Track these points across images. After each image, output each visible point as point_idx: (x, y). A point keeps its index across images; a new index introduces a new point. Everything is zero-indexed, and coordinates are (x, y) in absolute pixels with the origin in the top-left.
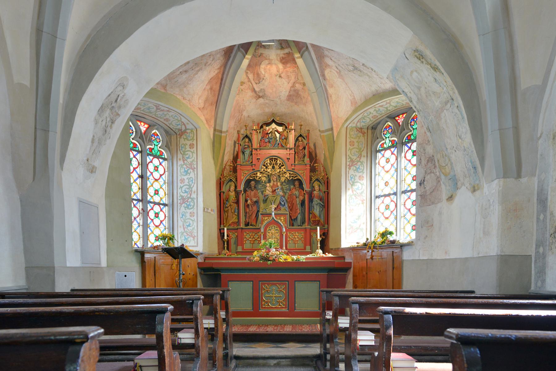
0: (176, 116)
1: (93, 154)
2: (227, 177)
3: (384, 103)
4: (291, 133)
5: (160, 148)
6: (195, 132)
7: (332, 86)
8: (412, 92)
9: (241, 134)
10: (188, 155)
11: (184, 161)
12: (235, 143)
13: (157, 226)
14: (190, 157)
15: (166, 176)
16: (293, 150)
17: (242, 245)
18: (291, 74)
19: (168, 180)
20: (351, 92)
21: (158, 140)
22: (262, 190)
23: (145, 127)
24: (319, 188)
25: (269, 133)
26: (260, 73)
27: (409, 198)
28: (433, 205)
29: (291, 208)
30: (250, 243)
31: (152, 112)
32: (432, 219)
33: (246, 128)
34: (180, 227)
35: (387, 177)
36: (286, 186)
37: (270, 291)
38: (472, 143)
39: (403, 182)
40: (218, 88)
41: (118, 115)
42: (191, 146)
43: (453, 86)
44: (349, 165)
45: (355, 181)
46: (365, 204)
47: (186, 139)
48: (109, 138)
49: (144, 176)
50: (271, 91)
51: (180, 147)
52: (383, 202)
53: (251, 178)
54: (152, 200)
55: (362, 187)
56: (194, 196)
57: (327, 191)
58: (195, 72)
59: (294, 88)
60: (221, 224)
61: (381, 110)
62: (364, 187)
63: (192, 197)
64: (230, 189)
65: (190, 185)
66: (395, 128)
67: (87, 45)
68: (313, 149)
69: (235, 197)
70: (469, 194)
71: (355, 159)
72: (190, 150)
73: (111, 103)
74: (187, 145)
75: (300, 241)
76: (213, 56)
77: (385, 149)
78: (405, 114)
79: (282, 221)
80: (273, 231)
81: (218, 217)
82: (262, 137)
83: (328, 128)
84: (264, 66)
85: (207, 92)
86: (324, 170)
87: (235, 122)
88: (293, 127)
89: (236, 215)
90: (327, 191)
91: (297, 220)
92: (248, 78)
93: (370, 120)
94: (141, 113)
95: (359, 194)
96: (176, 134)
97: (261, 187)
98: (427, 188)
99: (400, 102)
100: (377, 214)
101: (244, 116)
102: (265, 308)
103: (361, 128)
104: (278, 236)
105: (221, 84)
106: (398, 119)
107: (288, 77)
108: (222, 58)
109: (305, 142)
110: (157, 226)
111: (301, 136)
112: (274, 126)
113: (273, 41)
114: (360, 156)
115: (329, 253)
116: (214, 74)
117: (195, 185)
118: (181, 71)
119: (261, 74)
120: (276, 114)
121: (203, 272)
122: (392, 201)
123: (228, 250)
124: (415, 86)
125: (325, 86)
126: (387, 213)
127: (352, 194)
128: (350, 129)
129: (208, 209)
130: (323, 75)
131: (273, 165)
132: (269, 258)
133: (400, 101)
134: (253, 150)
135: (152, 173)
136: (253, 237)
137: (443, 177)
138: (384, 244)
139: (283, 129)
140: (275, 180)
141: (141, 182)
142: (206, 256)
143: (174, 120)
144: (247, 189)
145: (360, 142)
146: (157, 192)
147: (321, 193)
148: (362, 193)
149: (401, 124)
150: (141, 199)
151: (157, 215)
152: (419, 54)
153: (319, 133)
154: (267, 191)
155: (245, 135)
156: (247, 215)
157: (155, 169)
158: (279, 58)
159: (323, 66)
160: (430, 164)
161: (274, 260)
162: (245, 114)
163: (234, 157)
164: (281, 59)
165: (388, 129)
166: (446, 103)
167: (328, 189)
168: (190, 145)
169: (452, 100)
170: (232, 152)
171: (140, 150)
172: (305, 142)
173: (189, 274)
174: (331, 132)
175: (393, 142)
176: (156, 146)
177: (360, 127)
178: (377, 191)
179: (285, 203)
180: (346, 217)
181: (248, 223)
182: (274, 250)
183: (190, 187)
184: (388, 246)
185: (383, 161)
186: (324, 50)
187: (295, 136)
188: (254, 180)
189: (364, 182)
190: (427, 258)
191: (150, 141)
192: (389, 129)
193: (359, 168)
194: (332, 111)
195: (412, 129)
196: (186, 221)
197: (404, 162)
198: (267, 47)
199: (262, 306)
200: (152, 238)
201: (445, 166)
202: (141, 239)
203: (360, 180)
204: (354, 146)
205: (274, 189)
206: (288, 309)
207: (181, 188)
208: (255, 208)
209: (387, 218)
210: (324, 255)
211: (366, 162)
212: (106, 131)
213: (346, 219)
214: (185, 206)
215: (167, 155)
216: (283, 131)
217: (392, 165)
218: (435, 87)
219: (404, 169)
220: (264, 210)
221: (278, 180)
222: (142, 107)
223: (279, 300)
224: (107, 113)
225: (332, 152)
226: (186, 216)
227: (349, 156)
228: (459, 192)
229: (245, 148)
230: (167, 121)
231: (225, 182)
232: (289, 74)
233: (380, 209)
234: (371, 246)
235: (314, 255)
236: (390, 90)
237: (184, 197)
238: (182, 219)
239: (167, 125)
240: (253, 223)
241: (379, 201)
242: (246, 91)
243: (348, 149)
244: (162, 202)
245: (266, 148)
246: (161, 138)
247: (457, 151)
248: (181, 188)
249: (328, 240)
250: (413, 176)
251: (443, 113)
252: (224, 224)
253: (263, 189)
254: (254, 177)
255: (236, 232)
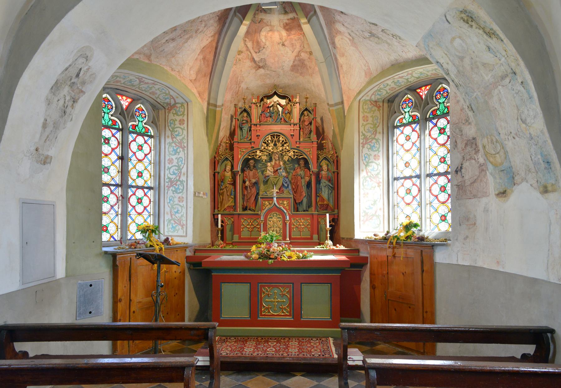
0: (163, 89)
1: (45, 141)
2: (222, 155)
3: (405, 74)
4: (295, 106)
5: (145, 124)
6: (186, 106)
7: (343, 55)
8: (450, 63)
9: (238, 108)
10: (178, 132)
11: (172, 138)
12: (232, 117)
13: (139, 214)
14: (180, 134)
15: (152, 155)
16: (298, 125)
17: (239, 233)
18: (296, 42)
19: (155, 160)
20: (365, 62)
21: (143, 116)
22: (262, 169)
23: (127, 102)
24: (328, 168)
25: (271, 107)
26: (259, 40)
27: (436, 182)
28: (476, 199)
29: (295, 190)
30: (248, 231)
31: (134, 84)
32: (475, 216)
33: (244, 101)
34: (167, 213)
35: (407, 157)
36: (290, 165)
37: (271, 294)
38: (545, 130)
39: (428, 163)
40: (212, 58)
41: (82, 92)
42: (181, 122)
43: (518, 56)
44: (362, 143)
45: (370, 161)
46: (381, 187)
47: (175, 114)
48: (70, 120)
49: (125, 157)
50: (272, 61)
51: (169, 123)
52: (403, 185)
53: (250, 157)
54: (134, 184)
55: (378, 167)
56: (183, 178)
57: (337, 171)
58: (184, 40)
59: (298, 58)
60: (215, 209)
61: (400, 82)
62: (380, 168)
63: (181, 179)
64: (226, 168)
65: (179, 166)
66: (417, 101)
67: (32, 6)
68: (320, 124)
69: (231, 177)
70: (536, 194)
71: (370, 136)
72: (180, 126)
73: (70, 79)
74: (176, 120)
75: (306, 228)
76: (205, 22)
77: (405, 125)
78: (429, 86)
79: (285, 205)
80: (274, 219)
81: (211, 202)
82: (263, 112)
83: (338, 101)
84: (265, 33)
85: (199, 62)
86: (332, 148)
87: (232, 95)
88: (297, 100)
89: (232, 198)
90: (337, 171)
91: (302, 205)
92: (247, 46)
93: (387, 93)
94: (122, 86)
95: (374, 176)
96: (165, 108)
97: (261, 166)
98: (466, 177)
99: (424, 73)
100: (396, 199)
101: (242, 88)
102: (265, 315)
103: (376, 102)
104: (281, 224)
105: (215, 53)
106: (420, 92)
107: (293, 45)
108: (216, 25)
109: (312, 117)
110: (139, 214)
111: (306, 109)
112: (276, 98)
113: (275, 3)
114: (375, 133)
115: (340, 244)
116: (207, 42)
117: (185, 166)
118: (167, 39)
119: (262, 42)
120: (278, 86)
121: (192, 267)
122: (414, 185)
123: (223, 240)
124: (457, 55)
125: (335, 55)
126: (408, 198)
127: (366, 175)
128: (364, 103)
129: (199, 193)
130: (333, 43)
131: (275, 142)
132: (270, 256)
133: (425, 72)
134: (252, 126)
135: (135, 153)
136: (252, 224)
137: (490, 167)
138: (409, 241)
139: (286, 102)
140: (277, 159)
141: (120, 165)
142: (196, 248)
143: (162, 94)
144: (245, 169)
145: (374, 117)
146: (140, 175)
147: (330, 174)
148: (378, 174)
149: (424, 97)
150: (120, 183)
151: (140, 201)
152: (468, 16)
153: (327, 107)
154: (268, 171)
155: (243, 109)
156: (245, 198)
157: (138, 148)
158: (282, 24)
159: (333, 32)
160: (469, 148)
161: (276, 258)
162: (243, 86)
163: (230, 132)
164: (285, 24)
165: (407, 103)
166: (503, 78)
167: (337, 169)
168: (180, 121)
169: (513, 75)
170: (229, 127)
171: (121, 127)
172: (312, 117)
173: (175, 272)
174: (341, 106)
175: (414, 117)
176: (140, 123)
177: (374, 100)
178: (395, 171)
179: (288, 185)
180: (360, 202)
181: (247, 207)
182: (276, 245)
183: (179, 168)
184: (415, 244)
185: (402, 139)
186: (336, 14)
187: (300, 109)
188: (253, 159)
189: (380, 161)
190: (468, 264)
191: (133, 118)
192: (409, 103)
193: (374, 146)
194: (342, 82)
195: (437, 103)
196: (174, 207)
197: (428, 141)
198: (268, 11)
199: (261, 313)
200: (133, 228)
201: (495, 154)
202: (119, 230)
203: (375, 159)
204: (368, 122)
205: (276, 169)
206: (293, 318)
207: (169, 169)
208: (254, 190)
209: (408, 204)
210: (335, 248)
211: (381, 139)
212: (65, 112)
213: (360, 204)
214: (174, 189)
215: (154, 132)
216: (287, 105)
217: (413, 143)
218: (488, 58)
219: (428, 149)
220: (264, 193)
221: (281, 159)
222: (121, 79)
223: (282, 306)
224: (66, 90)
225: (342, 128)
226: (174, 202)
227: (362, 132)
228: (517, 189)
229: (243, 123)
230: (154, 95)
231: (220, 161)
232: (294, 42)
233: (399, 193)
234: (392, 241)
235: (323, 247)
236: (413, 59)
237: (173, 180)
238: (169, 204)
239: (153, 99)
240: (251, 208)
241: (398, 184)
242: (245, 61)
243: (361, 125)
244: (146, 186)
245: (266, 123)
246: (146, 113)
247: (517, 138)
248: (169, 169)
249: (339, 228)
250: (440, 157)
251: (496, 90)
252: (218, 208)
253: (264, 169)
254: (253, 155)
255: (232, 218)
